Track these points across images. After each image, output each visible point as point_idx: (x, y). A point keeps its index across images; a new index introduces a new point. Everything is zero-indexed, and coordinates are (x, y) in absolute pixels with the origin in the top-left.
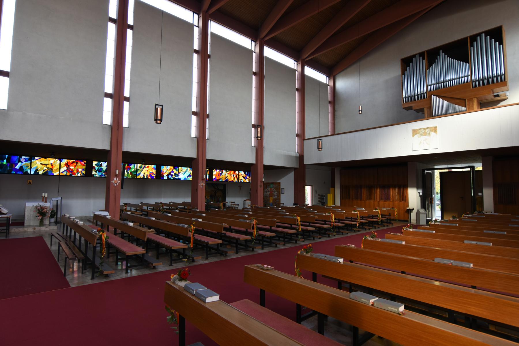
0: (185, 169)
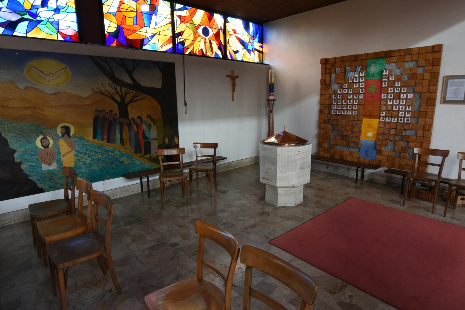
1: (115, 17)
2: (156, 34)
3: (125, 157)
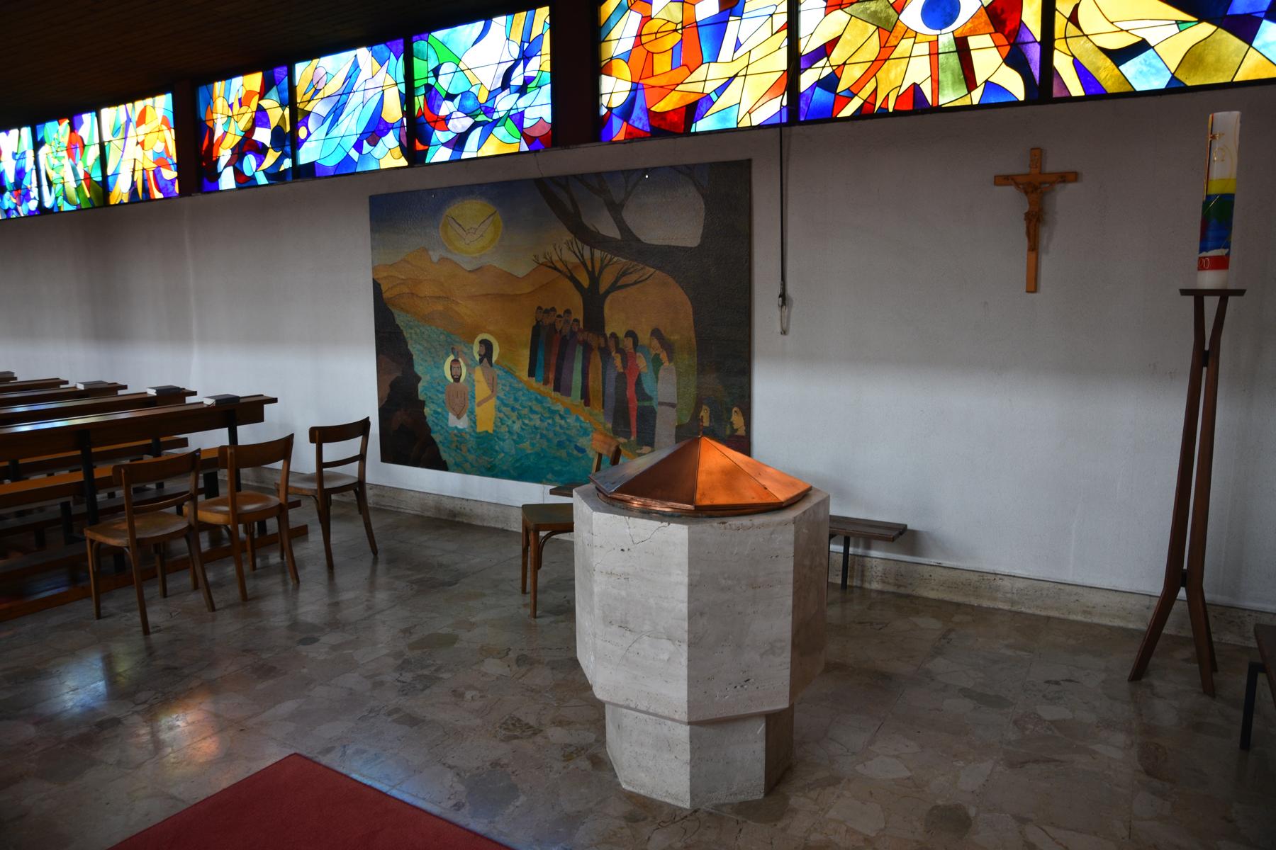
0: (334, 66)
1: (627, 63)
2: (736, 76)
3: (588, 438)
